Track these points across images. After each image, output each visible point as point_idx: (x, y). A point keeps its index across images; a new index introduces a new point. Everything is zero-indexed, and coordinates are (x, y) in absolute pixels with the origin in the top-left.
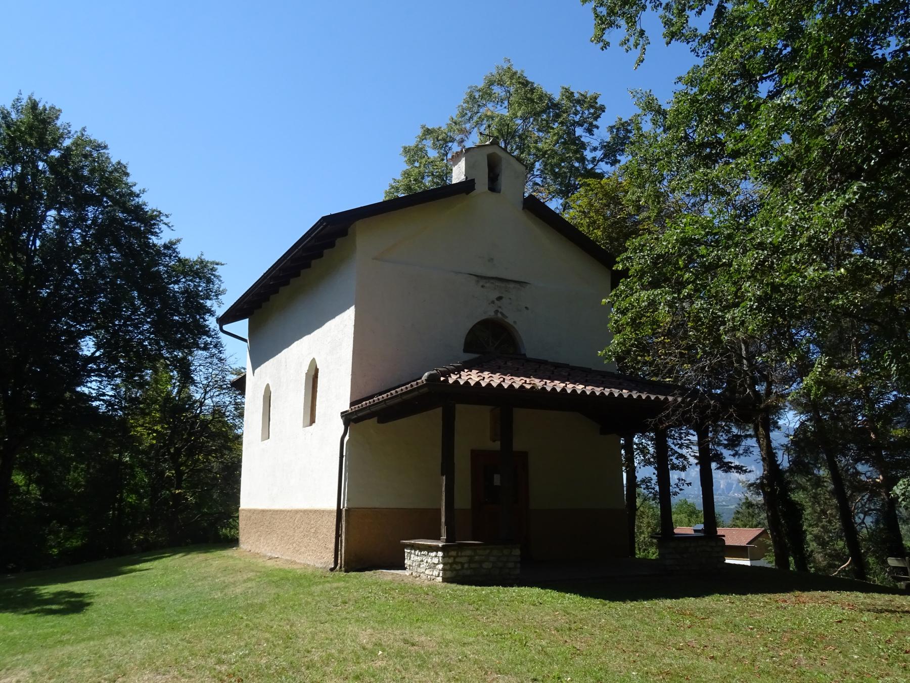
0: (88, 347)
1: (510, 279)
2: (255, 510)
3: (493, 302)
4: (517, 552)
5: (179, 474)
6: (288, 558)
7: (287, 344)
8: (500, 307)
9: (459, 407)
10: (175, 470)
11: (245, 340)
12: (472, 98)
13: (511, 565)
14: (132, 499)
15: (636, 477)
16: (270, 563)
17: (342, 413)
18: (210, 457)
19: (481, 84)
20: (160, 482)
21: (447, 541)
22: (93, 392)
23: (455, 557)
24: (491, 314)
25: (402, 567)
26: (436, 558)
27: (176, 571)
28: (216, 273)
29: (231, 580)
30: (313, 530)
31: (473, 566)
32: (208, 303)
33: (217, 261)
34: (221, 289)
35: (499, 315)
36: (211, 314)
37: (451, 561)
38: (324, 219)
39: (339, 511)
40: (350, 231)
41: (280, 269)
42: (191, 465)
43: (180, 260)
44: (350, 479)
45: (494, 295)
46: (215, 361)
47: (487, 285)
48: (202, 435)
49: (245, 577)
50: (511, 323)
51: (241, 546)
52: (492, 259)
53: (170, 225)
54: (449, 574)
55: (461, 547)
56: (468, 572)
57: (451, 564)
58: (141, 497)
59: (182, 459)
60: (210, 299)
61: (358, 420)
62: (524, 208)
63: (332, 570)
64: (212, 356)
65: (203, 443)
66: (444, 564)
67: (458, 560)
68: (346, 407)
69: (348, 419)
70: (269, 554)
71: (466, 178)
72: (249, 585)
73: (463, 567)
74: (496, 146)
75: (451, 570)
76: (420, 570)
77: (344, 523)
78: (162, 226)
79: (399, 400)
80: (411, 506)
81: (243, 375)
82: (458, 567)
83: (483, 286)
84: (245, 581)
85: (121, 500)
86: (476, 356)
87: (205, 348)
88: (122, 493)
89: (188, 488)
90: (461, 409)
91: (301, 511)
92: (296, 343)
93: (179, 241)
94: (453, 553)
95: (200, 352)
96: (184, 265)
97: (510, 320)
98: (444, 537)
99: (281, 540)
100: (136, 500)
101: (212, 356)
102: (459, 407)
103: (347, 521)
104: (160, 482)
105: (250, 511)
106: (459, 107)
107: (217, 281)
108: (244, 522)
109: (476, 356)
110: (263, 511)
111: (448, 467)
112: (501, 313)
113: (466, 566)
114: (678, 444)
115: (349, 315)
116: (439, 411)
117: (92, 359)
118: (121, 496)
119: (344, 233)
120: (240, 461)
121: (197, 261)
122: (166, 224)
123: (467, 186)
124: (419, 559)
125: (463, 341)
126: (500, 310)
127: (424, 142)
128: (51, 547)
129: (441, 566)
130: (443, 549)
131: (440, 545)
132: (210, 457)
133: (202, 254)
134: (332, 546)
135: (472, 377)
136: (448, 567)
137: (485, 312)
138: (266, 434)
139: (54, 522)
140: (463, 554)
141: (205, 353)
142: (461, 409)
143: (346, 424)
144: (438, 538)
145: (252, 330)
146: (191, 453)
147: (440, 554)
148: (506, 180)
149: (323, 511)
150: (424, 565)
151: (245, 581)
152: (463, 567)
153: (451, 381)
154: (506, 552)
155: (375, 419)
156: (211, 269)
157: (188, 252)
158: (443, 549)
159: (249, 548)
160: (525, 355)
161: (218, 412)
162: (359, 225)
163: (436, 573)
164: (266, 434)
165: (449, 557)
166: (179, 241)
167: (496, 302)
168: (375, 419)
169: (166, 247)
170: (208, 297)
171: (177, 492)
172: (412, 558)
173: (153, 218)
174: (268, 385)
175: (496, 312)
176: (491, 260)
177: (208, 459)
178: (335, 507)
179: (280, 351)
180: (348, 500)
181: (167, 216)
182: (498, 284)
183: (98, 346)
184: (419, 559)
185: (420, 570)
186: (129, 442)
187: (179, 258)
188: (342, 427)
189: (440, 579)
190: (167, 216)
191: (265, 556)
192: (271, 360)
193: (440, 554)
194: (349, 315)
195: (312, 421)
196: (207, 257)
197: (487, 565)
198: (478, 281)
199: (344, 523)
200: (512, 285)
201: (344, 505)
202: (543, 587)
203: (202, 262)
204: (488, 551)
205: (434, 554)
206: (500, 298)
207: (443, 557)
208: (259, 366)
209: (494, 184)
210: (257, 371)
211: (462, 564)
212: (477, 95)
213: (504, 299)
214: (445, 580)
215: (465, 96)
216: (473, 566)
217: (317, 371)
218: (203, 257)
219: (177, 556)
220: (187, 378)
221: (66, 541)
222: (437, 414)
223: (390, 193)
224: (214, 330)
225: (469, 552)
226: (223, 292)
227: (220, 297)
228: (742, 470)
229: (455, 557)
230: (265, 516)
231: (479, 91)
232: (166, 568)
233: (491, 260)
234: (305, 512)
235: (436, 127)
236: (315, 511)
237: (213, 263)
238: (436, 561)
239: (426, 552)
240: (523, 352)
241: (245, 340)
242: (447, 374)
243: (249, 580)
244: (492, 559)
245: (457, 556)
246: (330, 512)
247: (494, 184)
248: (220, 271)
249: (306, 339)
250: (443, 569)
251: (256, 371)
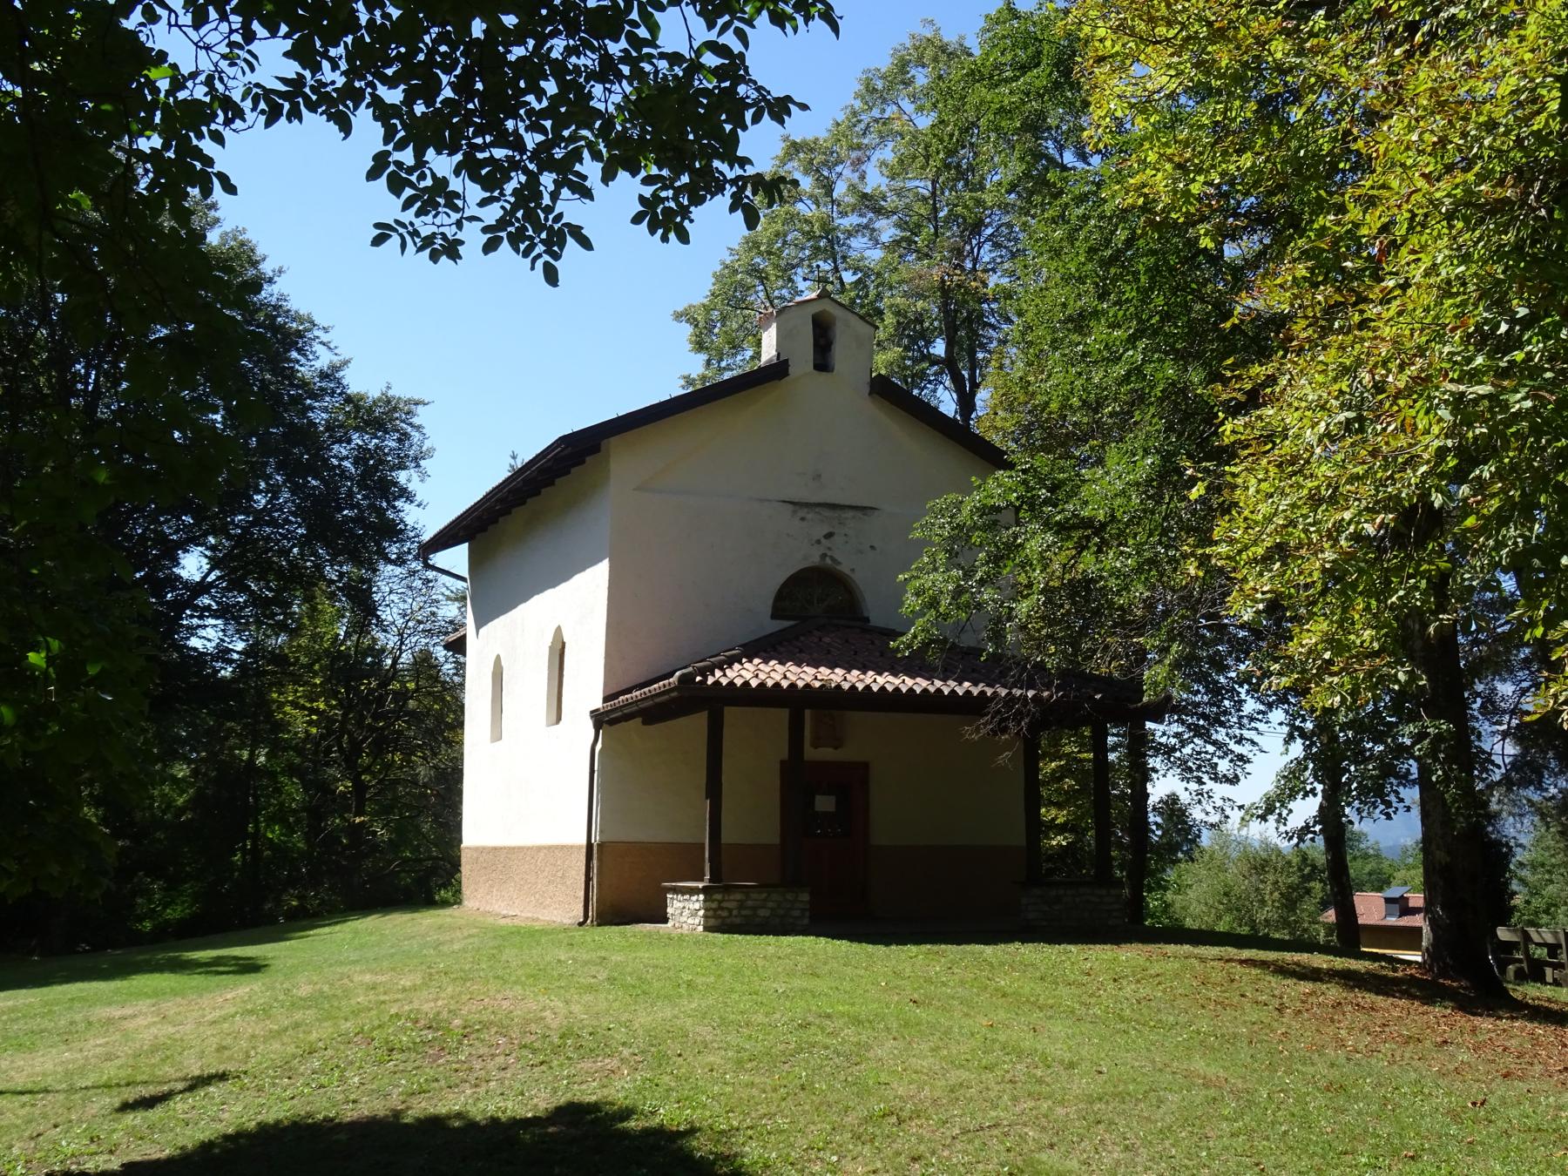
0: (193, 565)
1: (847, 503)
2: (484, 848)
3: (818, 542)
4: (805, 897)
5: (360, 787)
6: (530, 915)
7: (525, 598)
8: (829, 549)
9: (727, 710)
10: (352, 780)
11: (463, 579)
12: (870, 89)
13: (797, 913)
14: (274, 833)
15: (1148, 796)
16: (503, 922)
17: (592, 712)
18: (414, 758)
19: (885, 63)
20: (322, 801)
21: (710, 881)
22: (209, 645)
23: (720, 902)
24: (814, 559)
25: (665, 920)
26: (696, 902)
27: (371, 934)
28: (416, 421)
29: (448, 938)
30: (560, 874)
31: (744, 912)
32: (402, 477)
33: (416, 398)
34: (424, 449)
35: (828, 561)
36: (407, 498)
37: (714, 905)
38: (563, 440)
39: (589, 846)
40: (603, 447)
41: (509, 491)
42: (380, 772)
43: (349, 400)
44: (603, 801)
45: (820, 531)
46: (418, 583)
47: (809, 516)
48: (398, 718)
49: (466, 934)
50: (847, 571)
51: (465, 903)
52: (820, 476)
53: (332, 346)
54: (712, 922)
55: (727, 889)
56: (738, 921)
57: (715, 910)
58: (290, 830)
59: (365, 759)
60: (405, 468)
61: (612, 722)
62: (870, 394)
63: (581, 924)
64: (413, 573)
65: (400, 733)
66: (706, 910)
67: (724, 905)
68: (598, 703)
69: (600, 720)
70: (504, 912)
71: (778, 356)
72: (471, 940)
73: (731, 915)
74: (826, 300)
75: (714, 917)
76: (683, 919)
77: (595, 862)
78: (317, 348)
79: (649, 703)
80: (689, 840)
81: (458, 635)
82: (725, 914)
83: (803, 519)
84: (466, 938)
85: (256, 836)
86: (792, 623)
87: (400, 561)
88: (257, 823)
89: (374, 814)
90: (731, 714)
91: (544, 848)
92: (536, 597)
93: (346, 363)
94: (718, 896)
95: (390, 567)
96: (357, 408)
97: (845, 568)
98: (708, 877)
99: (520, 890)
100: (281, 834)
101: (413, 573)
102: (727, 710)
103: (599, 860)
104: (322, 801)
105: (476, 849)
106: (846, 107)
107: (416, 436)
108: (468, 867)
109: (792, 623)
110: (495, 849)
111: (714, 789)
112: (831, 558)
113: (735, 912)
114: (1235, 737)
115: (598, 576)
116: (705, 714)
117: (202, 587)
118: (257, 827)
119: (595, 449)
120: (461, 771)
121: (380, 400)
122: (323, 344)
123: (778, 370)
124: (681, 905)
125: (770, 602)
126: (829, 553)
127: (789, 166)
128: (141, 919)
129: (701, 913)
130: (705, 890)
131: (701, 885)
132: (414, 758)
133: (388, 388)
134: (582, 894)
135: (747, 673)
136: (710, 913)
137: (803, 556)
138: (497, 735)
139: (141, 873)
140: (732, 897)
141: (398, 570)
142: (731, 714)
143: (598, 727)
144: (702, 880)
145: (475, 561)
146: (379, 749)
147: (702, 897)
148: (841, 353)
149: (572, 847)
150: (686, 912)
151: (466, 938)
152: (731, 915)
153: (710, 680)
154: (789, 896)
155: (639, 720)
156: (408, 413)
157: (362, 382)
158: (705, 890)
159: (477, 905)
160: (867, 620)
161: (424, 662)
162: (614, 441)
163: (697, 921)
164: (497, 735)
165: (713, 901)
166: (346, 363)
167: (823, 540)
168: (639, 720)
169: (324, 376)
170: (402, 467)
171: (358, 820)
172: (675, 905)
173: (300, 334)
174: (498, 658)
175: (824, 556)
176: (817, 477)
177: (409, 761)
178: (584, 842)
179: (514, 607)
180: (601, 831)
181: (326, 330)
182: (827, 513)
183: (215, 564)
184: (681, 905)
185: (683, 919)
186: (267, 727)
187: (349, 396)
188: (592, 732)
189: (701, 928)
190: (326, 330)
191: (497, 915)
192: (502, 618)
193: (702, 897)
194: (598, 576)
195: (559, 719)
196: (400, 391)
197: (763, 913)
198: (794, 512)
199: (595, 862)
200: (850, 514)
201: (596, 839)
202: (851, 940)
203: (389, 402)
204: (764, 895)
205: (694, 898)
206: (829, 535)
207: (705, 901)
208: (486, 623)
209: (823, 362)
210: (482, 631)
211: (730, 911)
212: (880, 85)
213: (836, 537)
214: (706, 929)
215: (859, 87)
216: (744, 912)
217: (564, 644)
218: (390, 393)
219: (369, 918)
220: (364, 606)
221: (165, 908)
222: (697, 723)
223: (723, 276)
224: (414, 528)
225: (738, 896)
226: (427, 455)
227: (422, 463)
228: (1408, 781)
229: (720, 902)
230: (501, 858)
231: (884, 77)
232: (356, 932)
233: (817, 477)
234: (551, 849)
235: (810, 137)
236: (562, 847)
237: (407, 402)
238: (697, 906)
239: (687, 897)
240: (866, 615)
241: (463, 579)
242: (704, 672)
243: (470, 936)
244: (770, 904)
245: (723, 901)
246: (580, 847)
247: (823, 362)
248: (422, 416)
249: (549, 593)
250: (705, 916)
251: (481, 631)
